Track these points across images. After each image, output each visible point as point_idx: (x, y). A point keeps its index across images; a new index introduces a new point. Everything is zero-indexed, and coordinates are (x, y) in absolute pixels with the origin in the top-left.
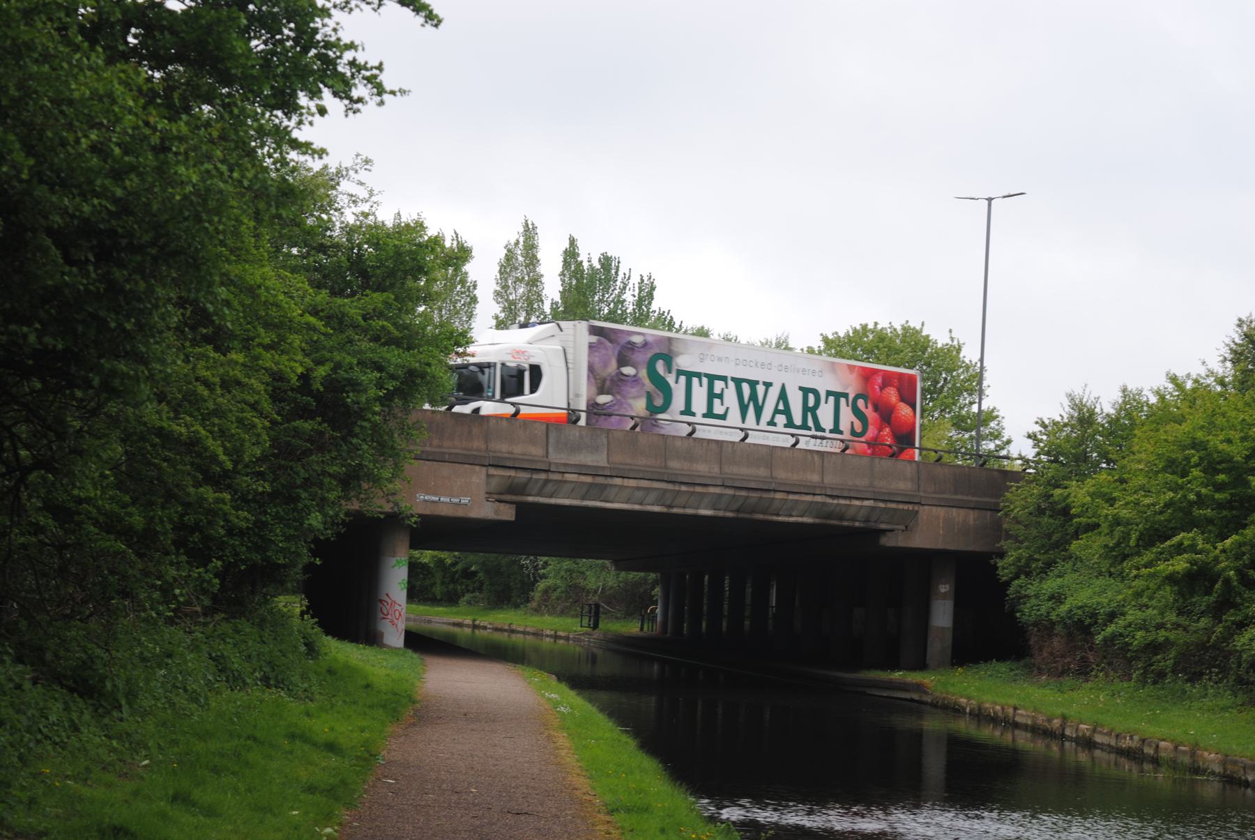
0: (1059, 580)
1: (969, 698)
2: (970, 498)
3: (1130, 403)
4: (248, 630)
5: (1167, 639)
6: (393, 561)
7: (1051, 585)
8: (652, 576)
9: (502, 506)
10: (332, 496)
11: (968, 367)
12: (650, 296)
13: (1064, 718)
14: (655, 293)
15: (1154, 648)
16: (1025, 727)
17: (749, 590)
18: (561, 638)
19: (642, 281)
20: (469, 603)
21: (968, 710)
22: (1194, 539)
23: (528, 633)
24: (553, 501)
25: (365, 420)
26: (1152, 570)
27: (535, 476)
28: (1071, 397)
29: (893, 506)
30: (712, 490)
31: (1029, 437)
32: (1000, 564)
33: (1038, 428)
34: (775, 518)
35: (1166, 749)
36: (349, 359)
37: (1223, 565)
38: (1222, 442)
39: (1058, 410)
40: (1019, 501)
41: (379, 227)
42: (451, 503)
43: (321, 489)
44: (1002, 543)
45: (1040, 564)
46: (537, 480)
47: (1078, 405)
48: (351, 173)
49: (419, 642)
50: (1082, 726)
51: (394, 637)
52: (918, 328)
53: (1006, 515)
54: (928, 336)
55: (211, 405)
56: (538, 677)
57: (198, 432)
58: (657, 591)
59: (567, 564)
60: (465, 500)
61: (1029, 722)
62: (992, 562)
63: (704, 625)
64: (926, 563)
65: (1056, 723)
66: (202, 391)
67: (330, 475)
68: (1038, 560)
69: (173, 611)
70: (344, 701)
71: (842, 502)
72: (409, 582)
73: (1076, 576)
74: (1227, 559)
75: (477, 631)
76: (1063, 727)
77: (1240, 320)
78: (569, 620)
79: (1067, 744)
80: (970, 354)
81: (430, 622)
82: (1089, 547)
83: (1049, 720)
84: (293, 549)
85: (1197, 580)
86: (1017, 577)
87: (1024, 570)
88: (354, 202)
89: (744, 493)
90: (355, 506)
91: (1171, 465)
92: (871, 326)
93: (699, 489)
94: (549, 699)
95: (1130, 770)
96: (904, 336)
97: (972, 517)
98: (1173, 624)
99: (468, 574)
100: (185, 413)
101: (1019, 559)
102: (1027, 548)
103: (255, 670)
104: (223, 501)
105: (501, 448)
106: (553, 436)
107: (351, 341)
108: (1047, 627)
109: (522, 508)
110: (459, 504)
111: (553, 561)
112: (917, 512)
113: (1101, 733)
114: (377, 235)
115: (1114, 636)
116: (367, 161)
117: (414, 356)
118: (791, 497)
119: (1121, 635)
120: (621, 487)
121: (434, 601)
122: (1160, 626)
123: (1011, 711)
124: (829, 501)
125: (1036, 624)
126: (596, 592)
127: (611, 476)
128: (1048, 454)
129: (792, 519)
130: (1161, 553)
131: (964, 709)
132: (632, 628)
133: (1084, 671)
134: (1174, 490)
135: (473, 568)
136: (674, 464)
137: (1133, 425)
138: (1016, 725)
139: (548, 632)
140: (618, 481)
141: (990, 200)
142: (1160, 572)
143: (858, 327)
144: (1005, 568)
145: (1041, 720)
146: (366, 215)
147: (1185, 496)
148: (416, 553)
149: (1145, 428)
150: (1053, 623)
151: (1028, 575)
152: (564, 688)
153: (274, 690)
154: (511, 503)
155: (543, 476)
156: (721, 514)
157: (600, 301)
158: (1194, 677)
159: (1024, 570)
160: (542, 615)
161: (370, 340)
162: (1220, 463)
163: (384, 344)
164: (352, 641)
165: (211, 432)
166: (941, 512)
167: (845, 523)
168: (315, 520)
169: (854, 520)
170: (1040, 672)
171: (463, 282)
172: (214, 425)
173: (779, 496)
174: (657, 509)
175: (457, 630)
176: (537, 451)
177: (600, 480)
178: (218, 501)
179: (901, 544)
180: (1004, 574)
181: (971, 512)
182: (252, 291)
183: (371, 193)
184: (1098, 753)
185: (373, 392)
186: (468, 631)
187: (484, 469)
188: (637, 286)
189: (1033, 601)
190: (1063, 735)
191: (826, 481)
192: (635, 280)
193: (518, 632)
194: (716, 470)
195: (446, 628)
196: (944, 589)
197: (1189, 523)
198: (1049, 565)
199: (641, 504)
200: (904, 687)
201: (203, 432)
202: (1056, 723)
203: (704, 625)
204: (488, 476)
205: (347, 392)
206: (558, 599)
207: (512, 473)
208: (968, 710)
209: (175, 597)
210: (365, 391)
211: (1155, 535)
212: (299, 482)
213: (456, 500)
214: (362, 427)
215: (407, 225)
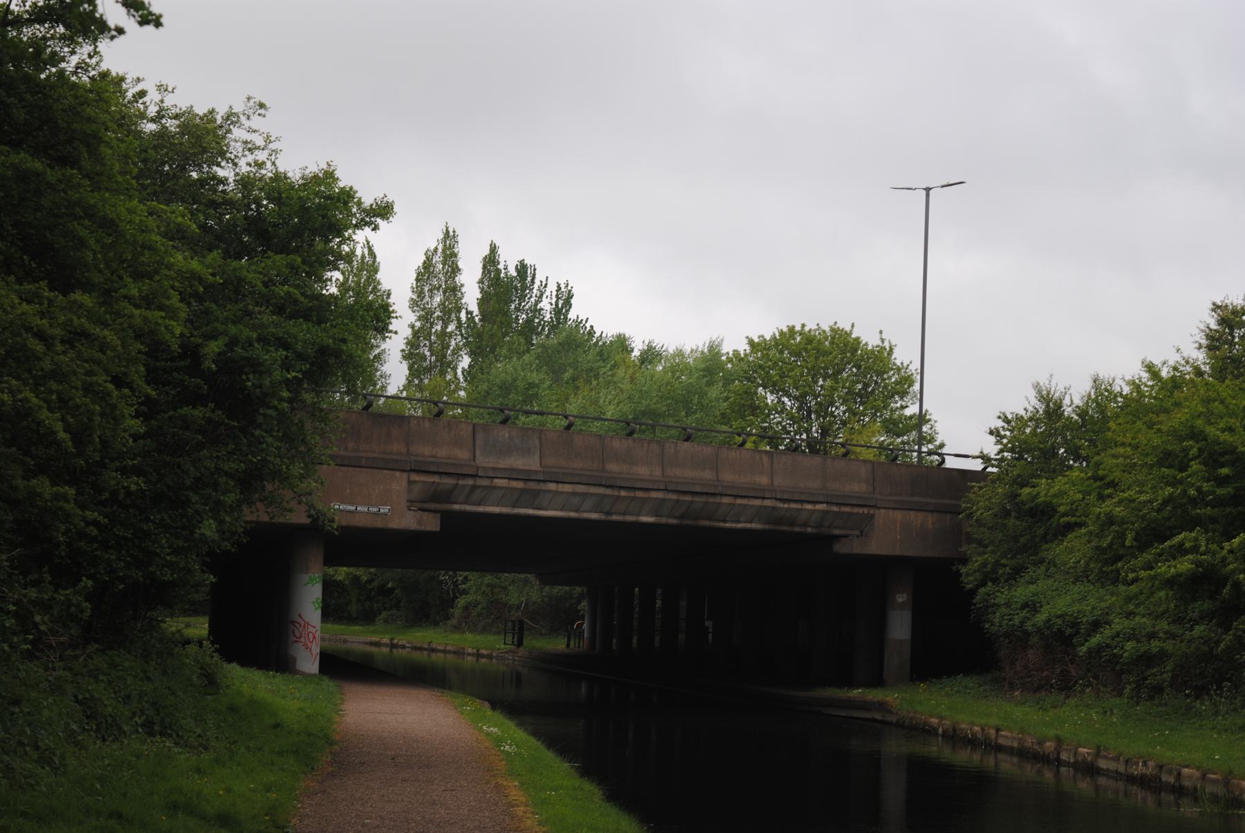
0: (1032, 588)
1: (941, 718)
2: (928, 500)
3: (1102, 394)
4: (127, 664)
5: (1162, 649)
6: (305, 578)
7: (1022, 592)
8: (578, 589)
9: (426, 516)
10: (229, 499)
11: (899, 369)
12: (568, 303)
13: (1059, 741)
14: (572, 301)
15: (1147, 660)
16: (1010, 751)
17: (683, 603)
18: (483, 656)
19: (559, 288)
20: (386, 621)
21: (940, 731)
22: (1196, 539)
23: (449, 652)
24: (481, 509)
25: (270, 408)
26: (1152, 573)
27: (461, 482)
28: (1037, 387)
29: (847, 509)
30: (654, 495)
31: (991, 433)
32: (963, 570)
33: (1000, 423)
34: (722, 525)
35: (1190, 777)
36: (247, 333)
37: (1231, 567)
38: (1223, 431)
39: (1022, 402)
40: (982, 504)
41: (279, 178)
42: (369, 513)
43: (216, 490)
44: (964, 549)
45: (1008, 570)
46: (464, 486)
47: (1045, 398)
48: (243, 119)
49: (342, 667)
50: (1081, 750)
51: (309, 663)
52: (848, 329)
53: (970, 516)
54: (858, 338)
55: (47, 365)
56: (472, 705)
57: (28, 401)
58: (584, 605)
59: (489, 579)
60: (385, 509)
61: (1015, 744)
62: (954, 568)
63: (635, 640)
64: (884, 570)
65: (1050, 745)
66: (38, 347)
67: (226, 474)
68: (1005, 566)
69: (32, 643)
70: (248, 748)
71: (793, 506)
72: (323, 600)
73: (1050, 582)
74: (1236, 559)
75: (395, 651)
76: (1058, 751)
77: (1214, 304)
78: (491, 638)
79: (1063, 769)
80: (905, 356)
81: (345, 641)
82: (1073, 550)
83: (1040, 743)
84: (182, 564)
85: (1204, 582)
86: (984, 584)
87: (989, 576)
88: (250, 150)
89: (688, 498)
90: (258, 514)
91: (1166, 458)
92: (798, 328)
93: (639, 494)
94: (488, 734)
95: (1144, 800)
96: (833, 338)
97: (930, 520)
98: (1166, 633)
99: (384, 591)
100: (9, 375)
101: (984, 565)
102: (993, 552)
103: (134, 714)
104: (65, 498)
105: (424, 451)
106: (480, 437)
107: (249, 314)
108: (1020, 638)
109: (448, 518)
110: (377, 514)
111: (473, 576)
112: (873, 516)
113: (1105, 757)
114: (278, 187)
115: (1100, 649)
116: (262, 106)
117: (325, 330)
118: (739, 501)
119: (1108, 646)
120: (556, 492)
121: (350, 619)
122: (1152, 636)
123: (993, 732)
124: (780, 505)
125: (1007, 635)
126: (518, 607)
127: (544, 481)
128: (1012, 450)
129: (740, 526)
130: (1160, 555)
131: (936, 730)
132: (558, 644)
133: (1066, 687)
134: (1173, 485)
135: (390, 585)
136: (613, 467)
137: (1105, 419)
138: (999, 748)
139: (470, 650)
140: (552, 486)
141: (928, 190)
142: (1160, 574)
143: (785, 330)
144: (969, 574)
145: (1029, 742)
146: (260, 165)
147: (1185, 492)
148: (331, 571)
149: (1120, 421)
150: (1027, 634)
151: (995, 581)
152: (498, 716)
153: (158, 738)
154: (435, 511)
155: (470, 482)
156: (663, 520)
157: (517, 309)
158: (1201, 692)
159: (989, 576)
160: (463, 632)
161: (273, 313)
162: (1222, 454)
163: (290, 317)
164: (260, 667)
165: (45, 401)
166: (898, 515)
167: (797, 529)
168: (209, 529)
169: (806, 525)
170: (1012, 687)
171: (375, 290)
172: (51, 392)
173: (726, 500)
174: (594, 516)
175: (374, 649)
176: (463, 454)
177: (532, 485)
178: (56, 497)
179: (857, 550)
180: (969, 582)
181: (930, 515)
182: (109, 225)
183: (268, 140)
184: (1102, 781)
185: (278, 375)
186: (386, 650)
187: (405, 475)
188: (554, 293)
189: (1004, 610)
190: (1058, 759)
191: (776, 483)
192: (552, 288)
193: (439, 651)
194: (658, 473)
195: (362, 648)
196: (901, 598)
197: (1191, 524)
198: (1018, 571)
199: (577, 511)
200: (865, 706)
201: (35, 400)
202: (1050, 745)
203: (635, 640)
204: (410, 482)
205: (247, 374)
206: (479, 615)
207: (436, 479)
208: (940, 731)
209: (36, 625)
210: (269, 373)
211: (1153, 534)
212: (188, 483)
213: (375, 510)
214: (265, 415)
215: (316, 177)
